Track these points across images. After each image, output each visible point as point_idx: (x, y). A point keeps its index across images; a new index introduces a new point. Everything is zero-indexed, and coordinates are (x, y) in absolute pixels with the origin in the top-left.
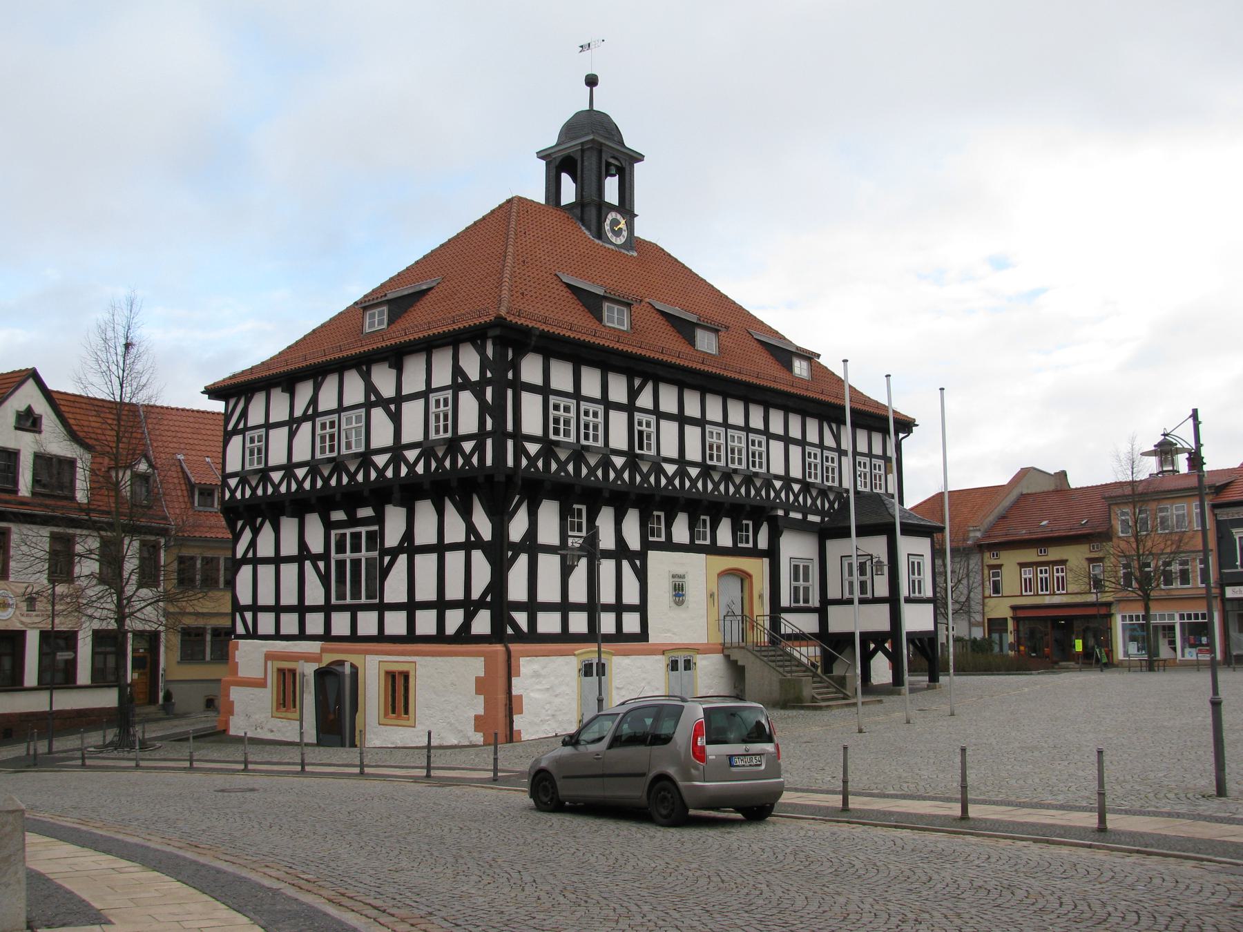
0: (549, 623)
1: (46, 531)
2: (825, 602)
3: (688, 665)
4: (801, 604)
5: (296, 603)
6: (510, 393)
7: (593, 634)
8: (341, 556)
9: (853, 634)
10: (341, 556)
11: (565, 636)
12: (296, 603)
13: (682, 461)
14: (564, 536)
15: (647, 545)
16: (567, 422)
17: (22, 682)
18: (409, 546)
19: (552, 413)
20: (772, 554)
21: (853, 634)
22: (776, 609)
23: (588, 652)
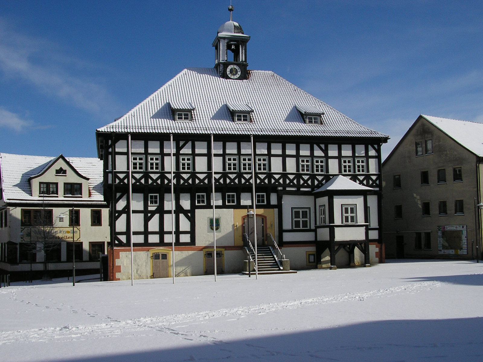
0: (135, 239)
1: (68, 209)
2: (317, 227)
3: (165, 256)
4: (350, 223)
5: (149, 230)
6: (110, 157)
7: (162, 243)
8: (347, 215)
9: (104, 242)
10: (347, 215)
11: (146, 244)
12: (149, 230)
13: (284, 175)
14: (146, 206)
15: (194, 207)
16: (249, 165)
17: (36, 261)
18: (127, 210)
19: (343, 164)
20: (279, 206)
21: (104, 242)
22: (281, 231)
23: (161, 250)
